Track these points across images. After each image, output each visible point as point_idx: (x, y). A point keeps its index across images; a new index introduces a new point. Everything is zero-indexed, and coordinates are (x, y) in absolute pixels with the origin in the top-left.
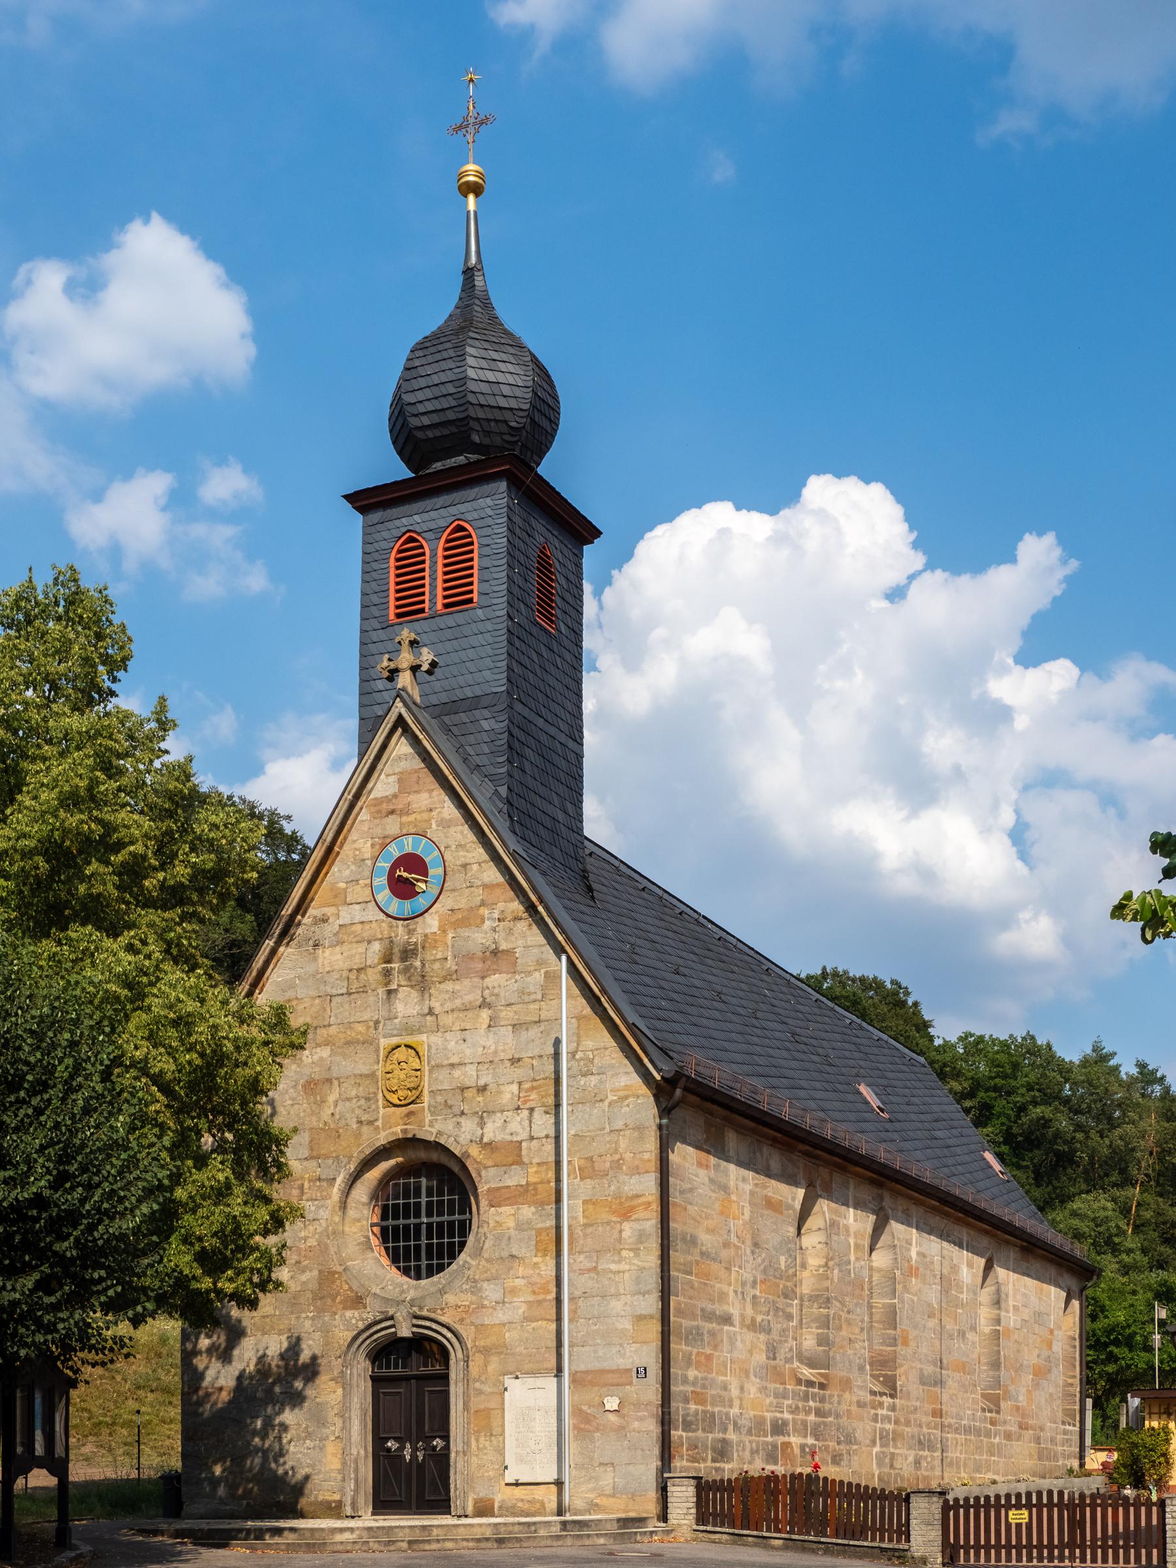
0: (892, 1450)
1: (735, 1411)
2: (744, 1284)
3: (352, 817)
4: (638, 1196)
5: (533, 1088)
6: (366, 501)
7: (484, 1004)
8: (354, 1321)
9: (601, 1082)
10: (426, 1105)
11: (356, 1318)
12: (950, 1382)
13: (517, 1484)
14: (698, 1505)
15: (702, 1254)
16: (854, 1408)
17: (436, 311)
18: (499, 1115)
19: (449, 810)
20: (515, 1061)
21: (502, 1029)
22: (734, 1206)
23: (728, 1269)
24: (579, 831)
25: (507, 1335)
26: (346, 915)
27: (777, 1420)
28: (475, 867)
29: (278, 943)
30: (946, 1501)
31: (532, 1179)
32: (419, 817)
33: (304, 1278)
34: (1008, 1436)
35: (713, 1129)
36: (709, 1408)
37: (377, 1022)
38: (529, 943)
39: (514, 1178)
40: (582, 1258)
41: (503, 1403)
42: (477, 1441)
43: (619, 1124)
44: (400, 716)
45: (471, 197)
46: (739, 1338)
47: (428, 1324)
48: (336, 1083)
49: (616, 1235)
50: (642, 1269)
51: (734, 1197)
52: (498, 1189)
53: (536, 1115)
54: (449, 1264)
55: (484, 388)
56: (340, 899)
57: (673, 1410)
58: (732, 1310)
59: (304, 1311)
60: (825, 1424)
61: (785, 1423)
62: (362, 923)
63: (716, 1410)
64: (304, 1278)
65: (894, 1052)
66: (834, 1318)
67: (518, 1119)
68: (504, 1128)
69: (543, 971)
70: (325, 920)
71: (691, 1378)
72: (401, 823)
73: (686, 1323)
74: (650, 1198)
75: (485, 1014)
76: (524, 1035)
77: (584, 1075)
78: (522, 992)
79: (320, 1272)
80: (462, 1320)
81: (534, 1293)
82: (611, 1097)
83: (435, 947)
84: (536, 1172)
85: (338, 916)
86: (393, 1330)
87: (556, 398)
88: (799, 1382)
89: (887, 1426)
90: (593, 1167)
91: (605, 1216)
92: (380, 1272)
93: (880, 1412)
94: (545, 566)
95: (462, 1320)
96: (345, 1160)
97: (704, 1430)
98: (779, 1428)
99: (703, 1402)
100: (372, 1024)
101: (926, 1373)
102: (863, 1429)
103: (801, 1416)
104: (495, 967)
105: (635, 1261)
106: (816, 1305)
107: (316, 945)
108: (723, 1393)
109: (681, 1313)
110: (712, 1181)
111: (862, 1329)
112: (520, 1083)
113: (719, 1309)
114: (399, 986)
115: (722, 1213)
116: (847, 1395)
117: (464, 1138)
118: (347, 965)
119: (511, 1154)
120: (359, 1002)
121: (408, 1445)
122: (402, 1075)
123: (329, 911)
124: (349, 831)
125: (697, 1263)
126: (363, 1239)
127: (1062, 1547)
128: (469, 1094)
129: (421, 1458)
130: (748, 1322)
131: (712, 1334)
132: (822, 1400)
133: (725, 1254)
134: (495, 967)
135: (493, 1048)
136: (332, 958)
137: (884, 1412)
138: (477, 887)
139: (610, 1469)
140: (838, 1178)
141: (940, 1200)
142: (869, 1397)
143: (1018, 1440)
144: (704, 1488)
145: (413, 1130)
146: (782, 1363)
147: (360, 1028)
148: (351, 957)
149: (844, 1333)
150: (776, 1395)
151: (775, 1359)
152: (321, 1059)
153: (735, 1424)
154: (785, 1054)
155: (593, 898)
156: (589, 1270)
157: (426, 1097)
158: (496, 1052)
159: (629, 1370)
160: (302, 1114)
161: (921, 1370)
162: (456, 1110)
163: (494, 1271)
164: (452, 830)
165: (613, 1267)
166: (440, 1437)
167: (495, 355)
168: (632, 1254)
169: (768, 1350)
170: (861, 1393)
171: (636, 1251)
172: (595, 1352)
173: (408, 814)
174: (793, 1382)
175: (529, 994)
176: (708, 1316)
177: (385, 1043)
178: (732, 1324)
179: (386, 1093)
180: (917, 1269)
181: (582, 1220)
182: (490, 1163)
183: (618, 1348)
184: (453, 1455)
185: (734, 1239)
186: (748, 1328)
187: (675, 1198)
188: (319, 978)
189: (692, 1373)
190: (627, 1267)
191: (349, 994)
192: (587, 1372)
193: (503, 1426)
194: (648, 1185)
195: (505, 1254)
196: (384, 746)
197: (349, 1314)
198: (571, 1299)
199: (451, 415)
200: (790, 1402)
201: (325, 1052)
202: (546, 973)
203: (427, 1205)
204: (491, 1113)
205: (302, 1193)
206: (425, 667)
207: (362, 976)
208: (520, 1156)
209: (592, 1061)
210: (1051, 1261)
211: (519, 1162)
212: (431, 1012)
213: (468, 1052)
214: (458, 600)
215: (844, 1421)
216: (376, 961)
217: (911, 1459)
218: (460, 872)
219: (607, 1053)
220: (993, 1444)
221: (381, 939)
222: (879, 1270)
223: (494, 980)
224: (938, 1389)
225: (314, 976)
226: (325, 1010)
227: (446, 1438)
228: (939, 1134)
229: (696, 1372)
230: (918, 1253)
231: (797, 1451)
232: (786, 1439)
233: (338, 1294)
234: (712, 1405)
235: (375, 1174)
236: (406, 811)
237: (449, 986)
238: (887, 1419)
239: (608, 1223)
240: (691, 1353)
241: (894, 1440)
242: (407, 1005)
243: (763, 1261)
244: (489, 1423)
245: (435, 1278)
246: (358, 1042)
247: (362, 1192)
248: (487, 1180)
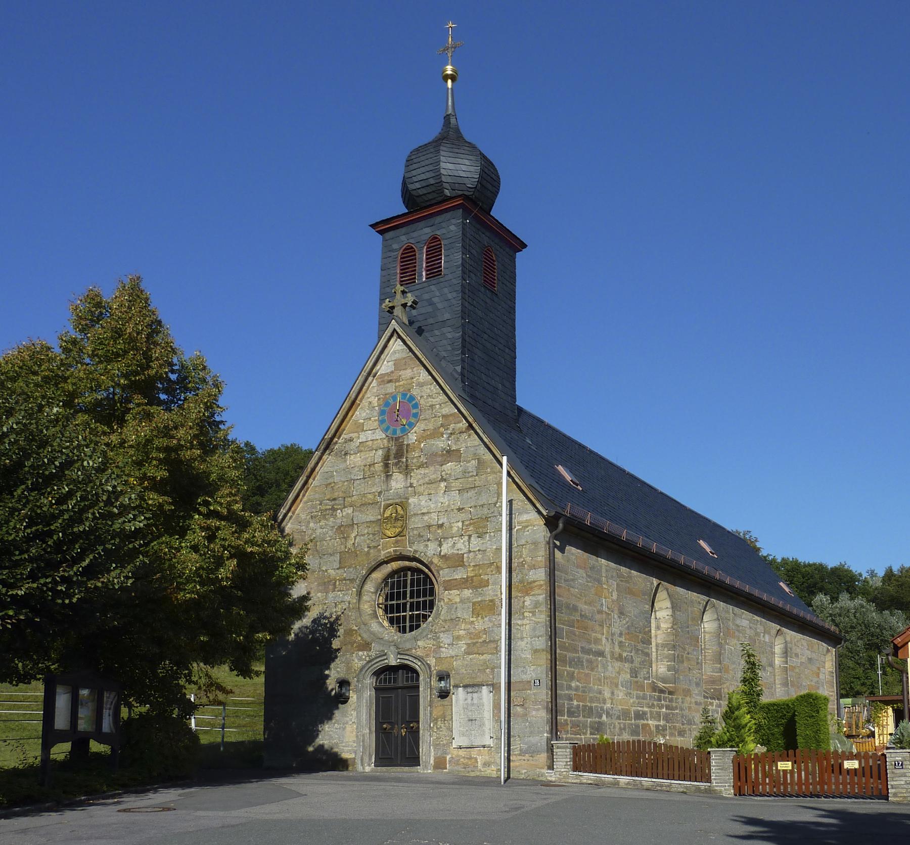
1: (608, 705)
2: (613, 635)
3: (366, 385)
4: (534, 582)
5: (470, 524)
7: (443, 480)
14: (574, 761)
16: (693, 705)
20: (459, 509)
28: (438, 406)
29: (323, 454)
39: (460, 574)
45: (449, 81)
47: (407, 657)
48: (356, 526)
49: (521, 604)
50: (537, 623)
53: (472, 539)
56: (360, 428)
60: (673, 714)
61: (645, 713)
63: (594, 705)
70: (351, 440)
73: (570, 655)
74: (542, 582)
75: (443, 484)
81: (471, 638)
83: (414, 451)
85: (359, 438)
97: (584, 716)
98: (639, 716)
99: (583, 700)
103: (656, 709)
107: (346, 454)
108: (598, 695)
112: (463, 522)
113: (594, 647)
115: (596, 594)
116: (688, 698)
117: (430, 553)
119: (457, 561)
123: (354, 435)
124: (366, 392)
125: (578, 621)
130: (616, 656)
131: (590, 662)
132: (671, 701)
136: (355, 460)
141: (747, 598)
144: (577, 751)
148: (366, 459)
149: (685, 664)
150: (638, 698)
151: (636, 677)
158: (449, 505)
159: (530, 682)
164: (425, 387)
167: (457, 151)
169: (631, 672)
171: (533, 613)
173: (399, 381)
174: (650, 690)
184: (421, 732)
186: (617, 659)
188: (348, 470)
191: (364, 478)
196: (385, 346)
197: (361, 653)
199: (432, 181)
203: (410, 593)
204: (446, 538)
207: (372, 469)
208: (463, 561)
211: (463, 565)
212: (411, 486)
213: (432, 506)
214: (434, 271)
215: (686, 712)
231: (653, 729)
232: (645, 722)
235: (378, 575)
236: (398, 380)
237: (422, 471)
240: (574, 672)
242: (398, 482)
246: (369, 504)
248: (444, 575)
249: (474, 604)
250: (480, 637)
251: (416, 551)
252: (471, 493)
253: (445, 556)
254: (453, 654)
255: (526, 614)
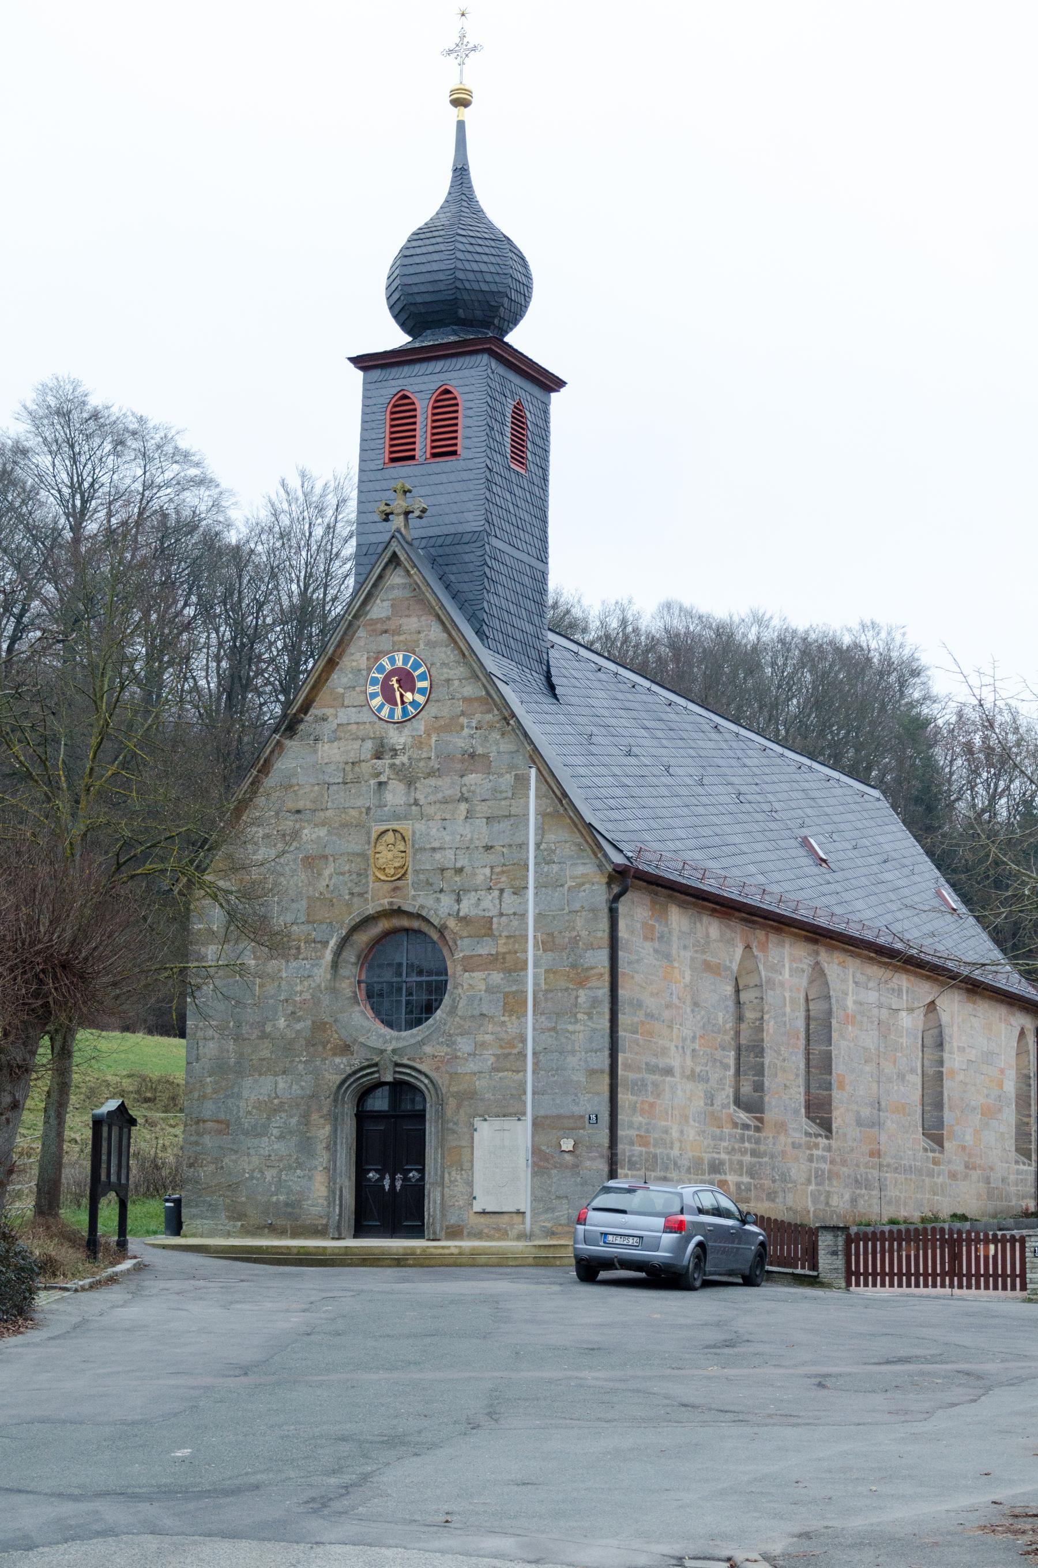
0: (827, 1189)
2: (684, 1040)
4: (592, 968)
5: (503, 872)
6: (364, 362)
7: (463, 799)
8: (342, 1066)
9: (561, 869)
10: (410, 882)
11: (343, 1064)
12: (889, 1123)
13: (484, 1213)
15: (647, 1015)
16: (789, 1149)
17: (426, 201)
18: (473, 893)
19: (436, 632)
20: (488, 848)
21: (478, 821)
22: (676, 971)
23: (670, 1027)
24: (541, 579)
25: (477, 1083)
26: (344, 716)
27: (715, 1159)
28: (456, 683)
30: (848, 1236)
31: (502, 950)
32: (408, 637)
33: (299, 1026)
34: (953, 1176)
35: (657, 907)
36: (652, 1150)
37: (369, 809)
38: (502, 750)
39: (485, 949)
40: (543, 1018)
41: (473, 1143)
42: (449, 1174)
43: (577, 906)
44: (395, 554)
46: (679, 1087)
47: (408, 1071)
48: (331, 859)
49: (572, 1001)
50: (594, 1030)
51: (676, 965)
52: (471, 957)
53: (505, 895)
54: (427, 1019)
55: (471, 276)
57: (619, 1151)
58: (673, 1063)
59: (298, 1056)
61: (722, 1163)
62: (358, 723)
64: (299, 1026)
65: (850, 791)
66: (769, 1067)
67: (490, 897)
68: (477, 905)
69: (513, 773)
70: (324, 719)
71: (636, 1125)
72: (394, 642)
73: (632, 1076)
74: (602, 970)
75: (463, 807)
76: (497, 827)
77: (548, 863)
78: (495, 790)
79: (313, 1022)
80: (438, 1069)
81: (501, 1047)
82: (570, 883)
84: (505, 944)
86: (376, 1075)
87: (528, 276)
88: (735, 1125)
89: (823, 1166)
90: (553, 942)
91: (563, 984)
92: (366, 1023)
93: (815, 1152)
94: (518, 413)
95: (438, 1069)
96: (338, 926)
99: (646, 1144)
100: (364, 810)
101: (863, 1115)
102: (798, 1170)
104: (472, 768)
105: (590, 1024)
106: (752, 1055)
108: (664, 1136)
109: (628, 1067)
110: (656, 951)
111: (797, 1075)
112: (492, 868)
113: (662, 1062)
114: (389, 779)
117: (443, 911)
118: (343, 759)
119: (485, 928)
120: (353, 791)
121: (387, 1176)
122: (390, 855)
123: (329, 711)
125: (643, 1023)
126: (351, 994)
127: (943, 1274)
128: (448, 874)
129: (398, 1188)
131: (655, 1085)
132: (758, 1142)
133: (667, 1014)
134: (472, 768)
135: (469, 836)
136: (330, 752)
137: (820, 1152)
138: (458, 699)
139: (564, 1201)
140: (773, 938)
141: (876, 952)
142: (804, 1139)
143: (964, 1180)
145: (398, 902)
146: (719, 1108)
147: (354, 813)
148: (347, 752)
150: (714, 1138)
151: (712, 1105)
152: (319, 837)
153: (675, 1164)
154: (727, 819)
155: (555, 696)
156: (549, 1030)
157: (410, 876)
158: (471, 840)
159: (582, 1117)
160: (300, 884)
161: (858, 1112)
162: (437, 888)
163: (466, 1027)
164: (437, 650)
165: (570, 1028)
166: (416, 1170)
168: (586, 1017)
169: (706, 1098)
170: (797, 1135)
171: (590, 1015)
172: (553, 1100)
173: (399, 634)
175: (501, 792)
176: (652, 1069)
177: (376, 829)
178: (673, 1075)
179: (375, 870)
180: (854, 1017)
181: (543, 987)
182: (465, 934)
183: (573, 1097)
185: (675, 1001)
186: (688, 1078)
187: (623, 968)
189: (638, 1119)
190: (582, 1028)
192: (546, 1117)
193: (472, 1161)
194: (602, 958)
195: (477, 1013)
197: (337, 1060)
198: (534, 1054)
200: (726, 1144)
201: (322, 832)
202: (516, 775)
205: (299, 953)
206: (417, 513)
207: (357, 769)
208: (491, 929)
209: (554, 851)
210: (1002, 1002)
212: (416, 803)
213: (447, 838)
214: (445, 449)
216: (369, 756)
217: (847, 1197)
218: (443, 685)
219: (567, 845)
220: (936, 1184)
221: (374, 738)
222: (816, 1019)
223: (472, 778)
224: (875, 1130)
225: (314, 766)
226: (323, 795)
227: (422, 1171)
228: (888, 876)
229: (640, 1119)
230: (855, 1002)
233: (328, 1042)
234: (655, 1146)
236: (398, 632)
237: (432, 781)
238: (823, 1159)
239: (566, 989)
241: (830, 1179)
243: (703, 1018)
244: (464, 1164)
245: (415, 1031)
247: (350, 955)
249: (506, 995)
250: (514, 1047)
251: (422, 907)
252: (505, 825)
253: (465, 918)
254: (476, 1069)
255: (580, 1016)
